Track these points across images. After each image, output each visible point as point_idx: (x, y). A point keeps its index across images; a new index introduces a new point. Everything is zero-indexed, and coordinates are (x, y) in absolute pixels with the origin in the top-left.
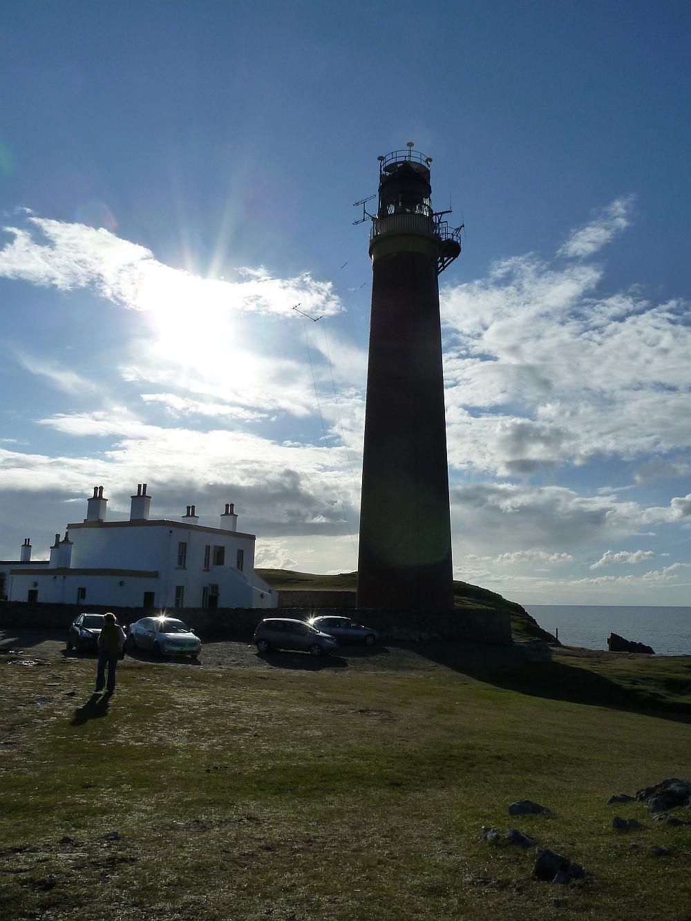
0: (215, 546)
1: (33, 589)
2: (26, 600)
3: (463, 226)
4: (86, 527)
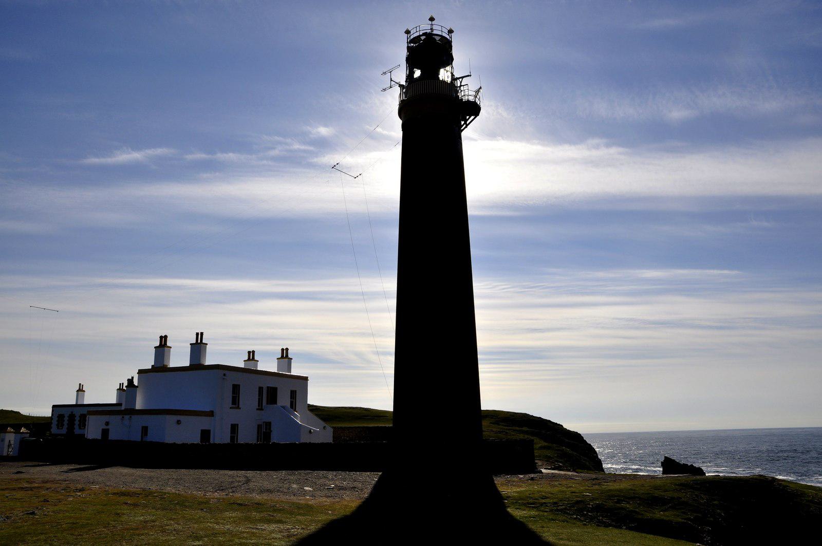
0: (268, 387)
1: (105, 427)
2: (100, 438)
3: (481, 88)
4: (153, 372)
